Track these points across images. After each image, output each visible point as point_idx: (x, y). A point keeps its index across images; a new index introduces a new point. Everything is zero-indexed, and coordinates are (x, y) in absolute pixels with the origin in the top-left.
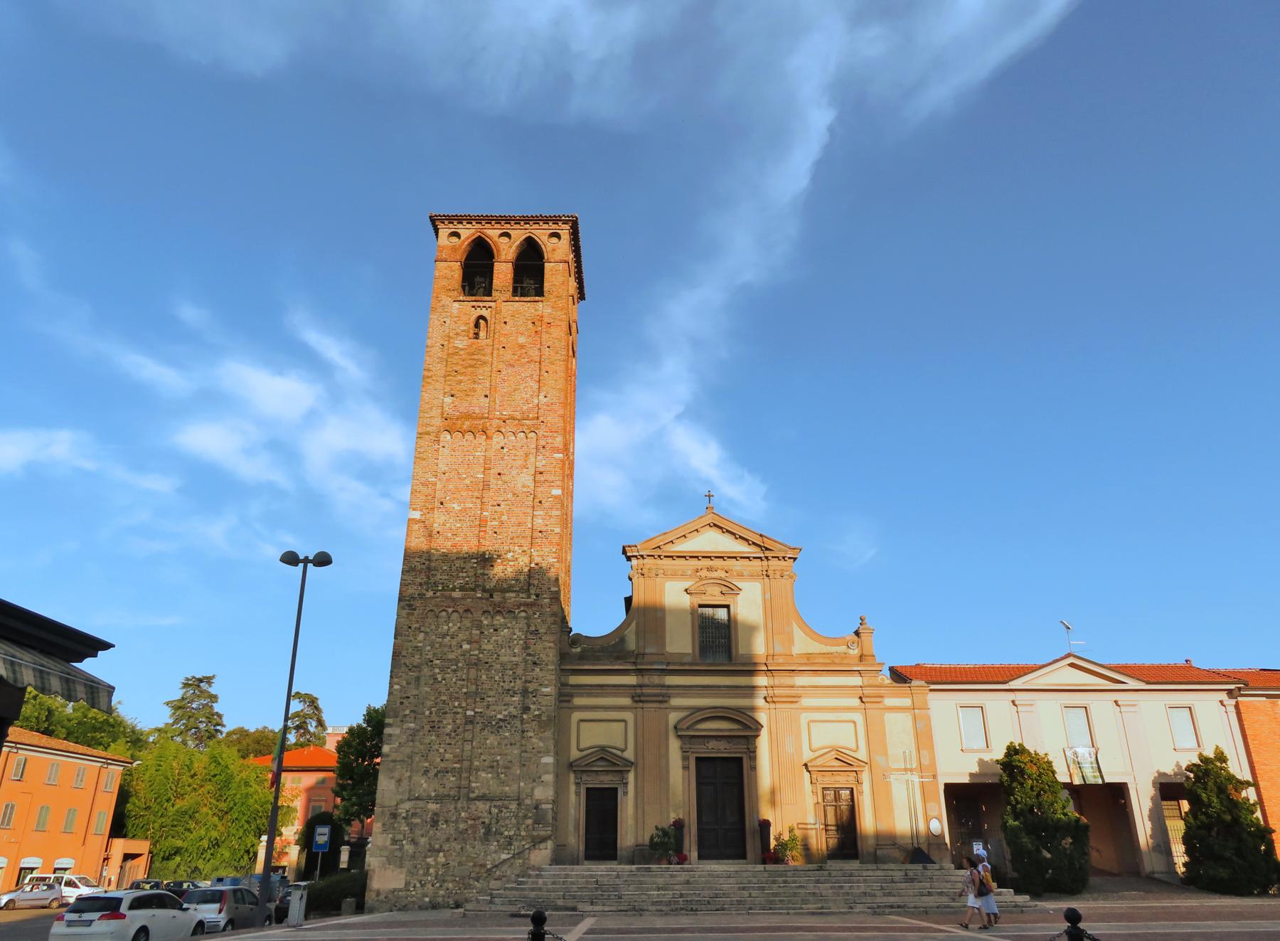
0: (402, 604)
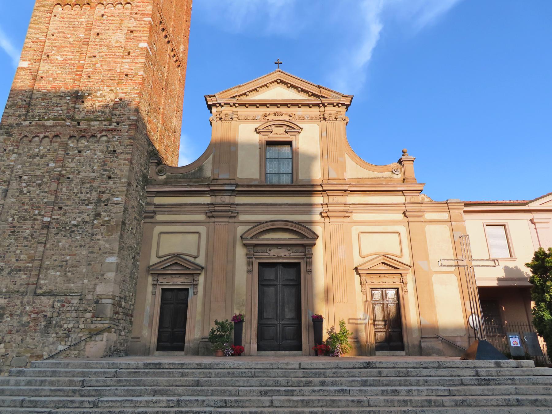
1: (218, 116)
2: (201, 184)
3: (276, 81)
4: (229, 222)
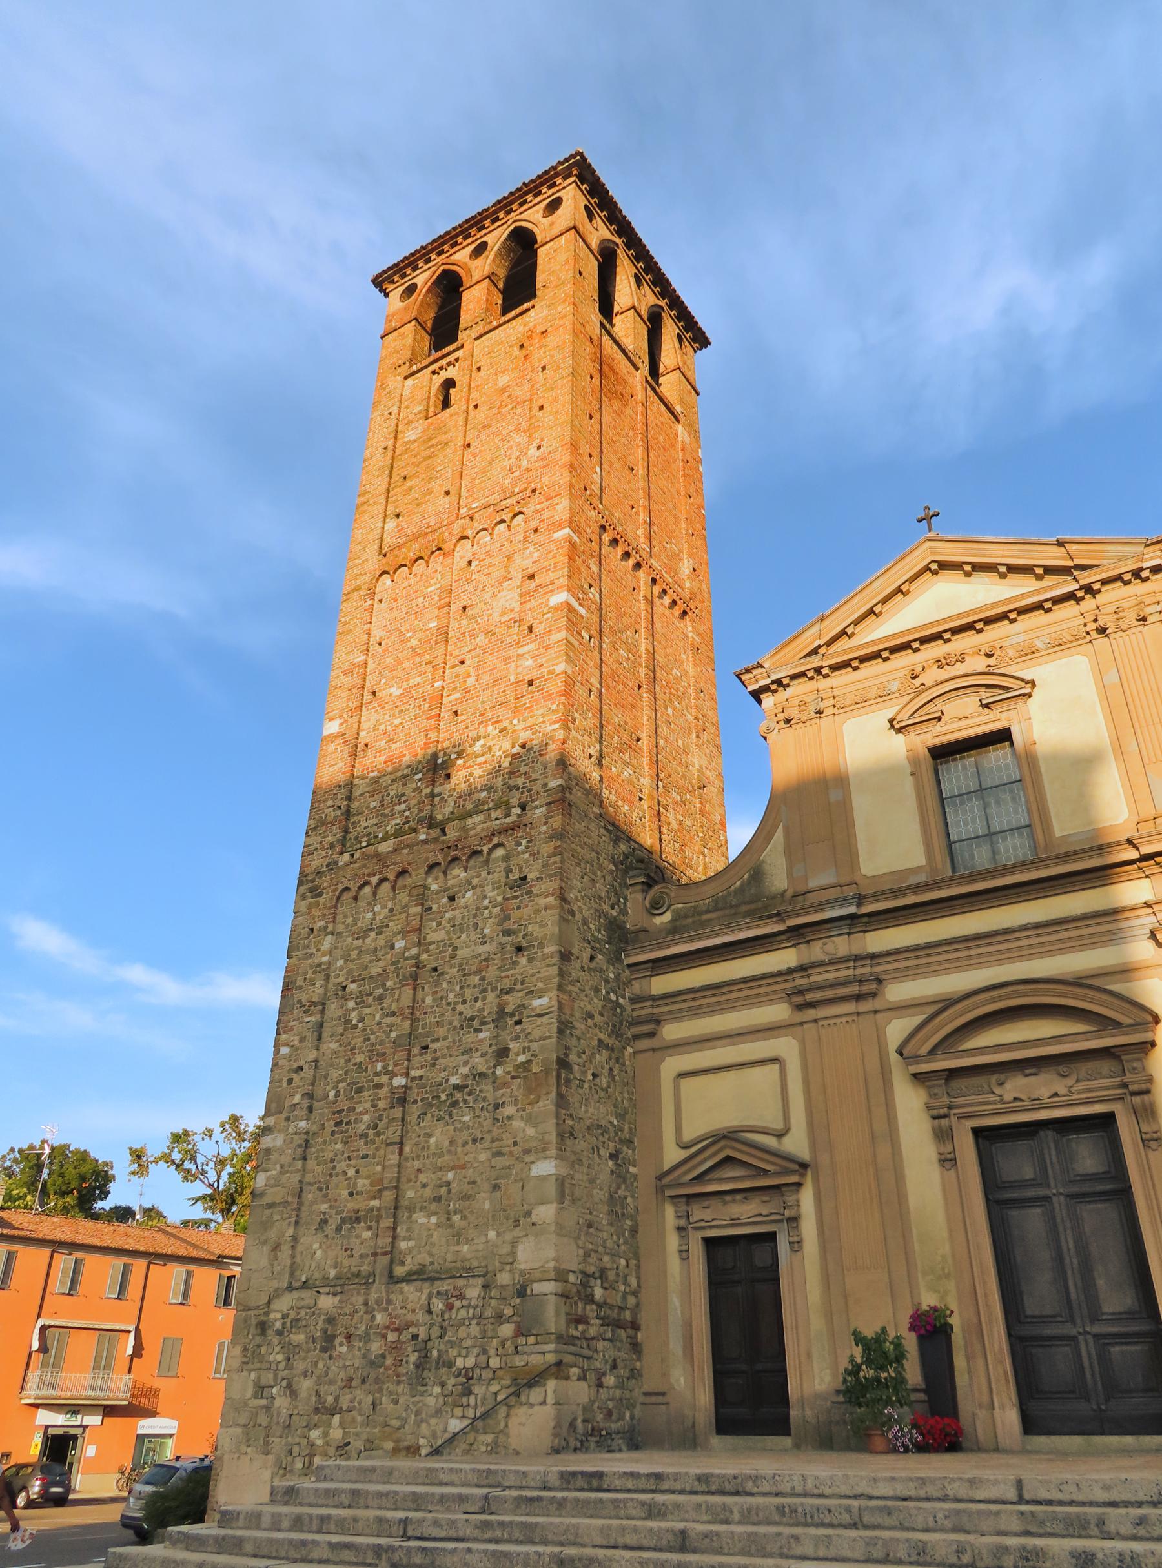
0: (303, 889)
1: (781, 716)
2: (760, 914)
3: (927, 568)
4: (858, 1014)
